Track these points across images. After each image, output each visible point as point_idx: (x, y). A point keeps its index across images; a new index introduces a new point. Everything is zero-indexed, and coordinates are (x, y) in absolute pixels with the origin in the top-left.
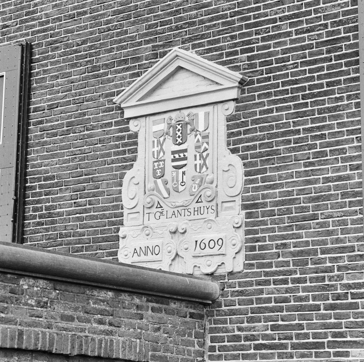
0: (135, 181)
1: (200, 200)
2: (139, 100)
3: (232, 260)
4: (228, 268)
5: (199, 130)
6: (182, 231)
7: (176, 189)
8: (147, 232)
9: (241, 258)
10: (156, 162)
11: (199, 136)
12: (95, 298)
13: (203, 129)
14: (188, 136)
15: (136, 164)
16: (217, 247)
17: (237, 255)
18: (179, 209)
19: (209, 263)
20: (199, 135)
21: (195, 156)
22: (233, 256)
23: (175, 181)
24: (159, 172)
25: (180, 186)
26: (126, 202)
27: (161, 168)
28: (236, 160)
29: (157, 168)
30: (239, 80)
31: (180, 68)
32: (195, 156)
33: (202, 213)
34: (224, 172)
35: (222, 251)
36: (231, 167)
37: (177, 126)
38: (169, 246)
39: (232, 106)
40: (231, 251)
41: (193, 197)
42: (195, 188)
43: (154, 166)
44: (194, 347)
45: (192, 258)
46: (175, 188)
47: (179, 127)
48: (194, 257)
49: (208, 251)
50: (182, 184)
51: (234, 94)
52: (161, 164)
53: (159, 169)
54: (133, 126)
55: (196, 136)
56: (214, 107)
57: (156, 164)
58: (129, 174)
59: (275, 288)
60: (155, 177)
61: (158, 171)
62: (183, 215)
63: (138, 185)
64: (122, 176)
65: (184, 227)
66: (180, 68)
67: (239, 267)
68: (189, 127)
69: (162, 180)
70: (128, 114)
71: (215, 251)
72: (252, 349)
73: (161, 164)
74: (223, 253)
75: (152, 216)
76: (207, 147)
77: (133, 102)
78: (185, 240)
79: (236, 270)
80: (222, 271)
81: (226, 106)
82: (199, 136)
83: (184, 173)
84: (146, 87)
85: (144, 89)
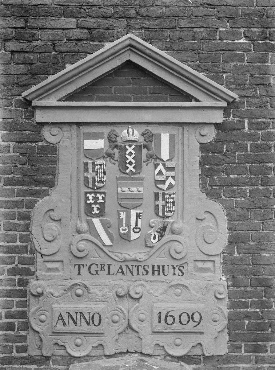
2: (69, 97)
5: (163, 158)
11: (161, 167)
14: (144, 164)
15: (52, 191)
16: (191, 323)
18: (129, 264)
20: (161, 164)
22: (214, 336)
23: (124, 225)
24: (95, 209)
25: (132, 232)
27: (100, 204)
28: (217, 207)
29: (93, 202)
33: (166, 274)
34: (197, 220)
35: (199, 328)
37: (127, 147)
38: (118, 315)
42: (155, 238)
45: (152, 333)
46: (124, 234)
47: (130, 149)
48: (203, 333)
51: (218, 117)
52: (100, 198)
53: (95, 203)
55: (156, 166)
57: (91, 196)
58: (42, 204)
62: (135, 273)
64: (31, 205)
67: (223, 349)
68: (144, 151)
70: (40, 117)
73: (100, 198)
74: (202, 331)
76: (173, 183)
77: (52, 101)
78: (41, 309)
81: (205, 131)
82: (161, 167)
83: (138, 216)
84: (85, 76)
85: (58, 92)
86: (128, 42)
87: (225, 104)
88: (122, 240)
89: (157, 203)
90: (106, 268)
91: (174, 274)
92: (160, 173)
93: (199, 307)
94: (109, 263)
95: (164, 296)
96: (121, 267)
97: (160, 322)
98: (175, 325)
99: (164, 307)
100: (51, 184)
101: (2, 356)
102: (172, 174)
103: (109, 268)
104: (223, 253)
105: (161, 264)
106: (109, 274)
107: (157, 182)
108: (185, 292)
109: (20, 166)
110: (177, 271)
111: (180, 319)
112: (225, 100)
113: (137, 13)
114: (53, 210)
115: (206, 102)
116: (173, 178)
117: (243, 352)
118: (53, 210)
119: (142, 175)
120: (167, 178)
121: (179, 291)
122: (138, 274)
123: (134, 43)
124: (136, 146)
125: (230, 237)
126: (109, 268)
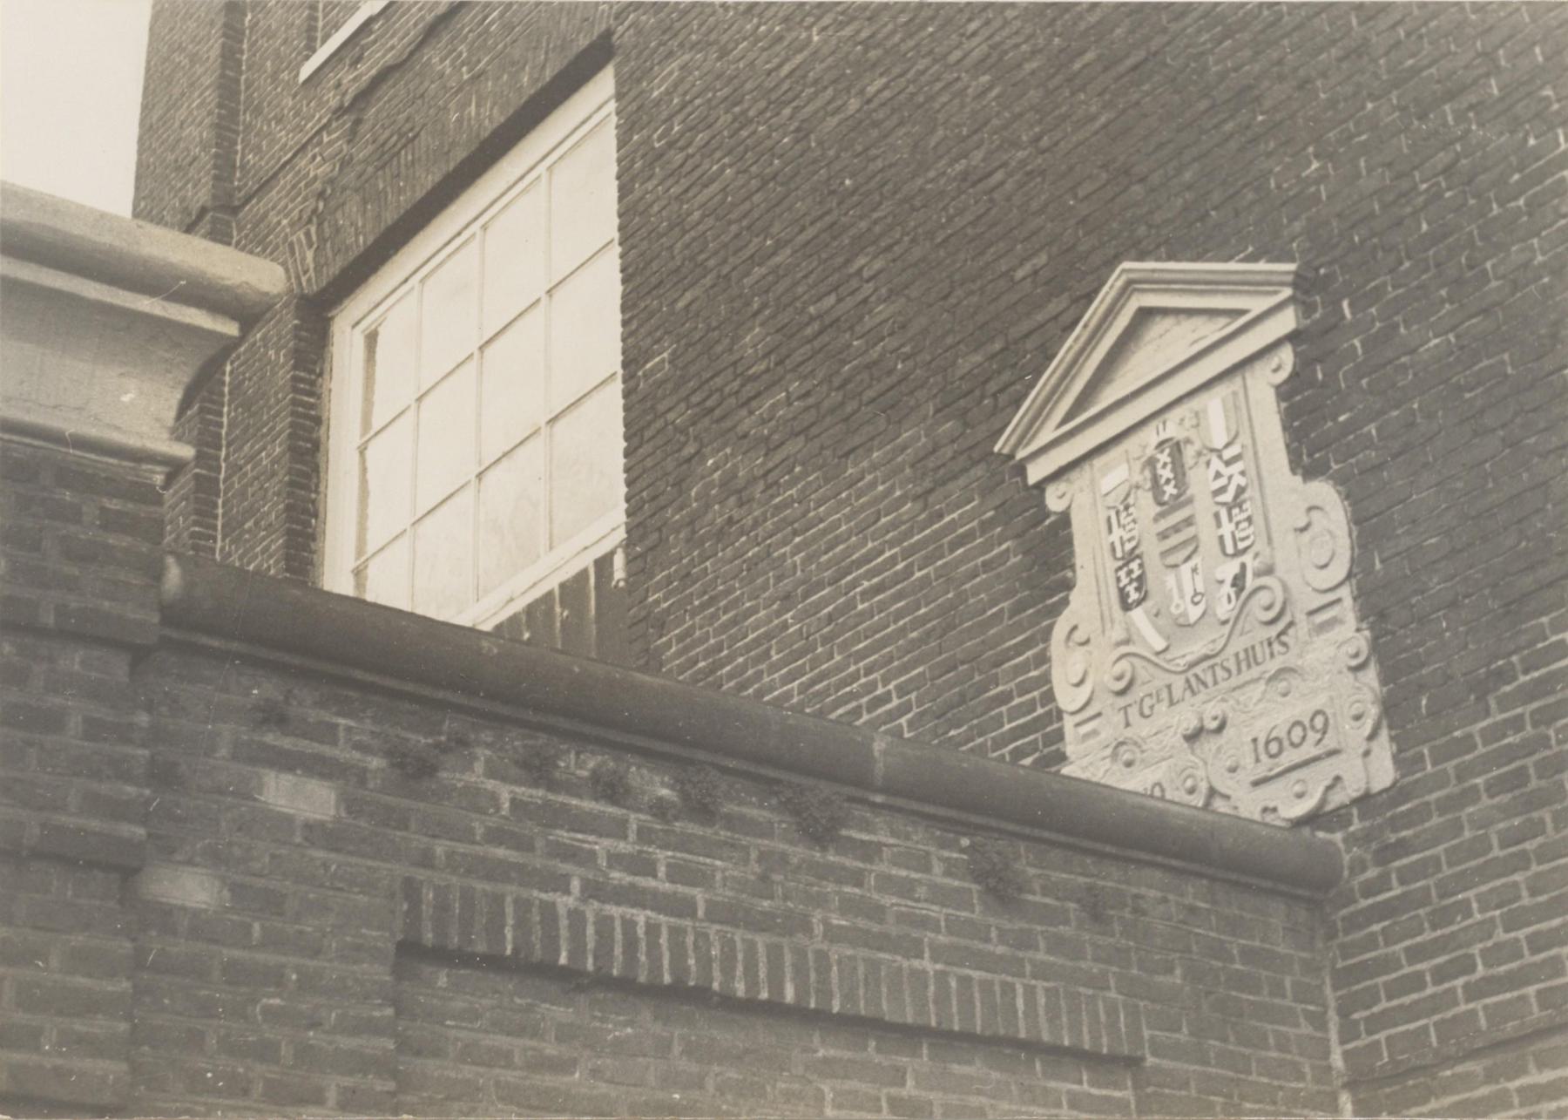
0: (1079, 636)
1: (1246, 629)
3: (1359, 762)
4: (1352, 789)
6: (1214, 725)
7: (1181, 621)
8: (1127, 756)
9: (1384, 750)
10: (1120, 568)
12: (530, 55)
13: (1225, 440)
15: (1074, 596)
16: (1313, 737)
17: (1375, 745)
18: (1198, 670)
19: (1298, 788)
21: (1217, 516)
22: (1361, 751)
26: (1068, 699)
28: (1324, 491)
30: (1290, 278)
31: (1146, 315)
32: (1217, 516)
33: (1260, 660)
35: (1330, 742)
36: (1315, 515)
39: (1286, 356)
40: (1353, 735)
41: (1228, 627)
43: (1118, 580)
44: (1297, 1025)
49: (1290, 757)
50: (1196, 599)
51: (1286, 322)
53: (1131, 581)
54: (1054, 500)
55: (1208, 464)
56: (1244, 379)
57: (1122, 574)
59: (1493, 807)
60: (1126, 606)
61: (1131, 589)
63: (1086, 648)
65: (1218, 711)
66: (1146, 315)
67: (1383, 773)
69: (1147, 612)
70: (1035, 473)
71: (1308, 750)
72: (1435, 814)
75: (1133, 712)
79: (1377, 786)
80: (1337, 799)
83: (1194, 570)
86: (1124, 278)
87: (1287, 292)
88: (1185, 629)
89: (1220, 532)
90: (1165, 695)
91: (1272, 655)
92: (1218, 475)
93: (1320, 701)
94: (1167, 682)
95: (1261, 706)
96: (1188, 681)
97: (1258, 760)
98: (1285, 754)
99: (1260, 729)
100: (1068, 585)
101: (1135, 1116)
102: (1239, 466)
103: (1170, 693)
104: (1349, 576)
105: (1249, 645)
106: (1172, 703)
107: (1217, 492)
108: (1295, 681)
109: (1024, 575)
110: (1277, 647)
111: (1290, 739)
112: (1283, 284)
113: (1150, 227)
114: (1075, 628)
115: (1257, 305)
116: (1243, 473)
117: (1429, 767)
118: (1075, 628)
119: (1189, 493)
120: (1230, 478)
121: (1284, 684)
122: (1216, 683)
123: (1132, 276)
124: (1171, 447)
125: (622, 265)
126: (1170, 693)
